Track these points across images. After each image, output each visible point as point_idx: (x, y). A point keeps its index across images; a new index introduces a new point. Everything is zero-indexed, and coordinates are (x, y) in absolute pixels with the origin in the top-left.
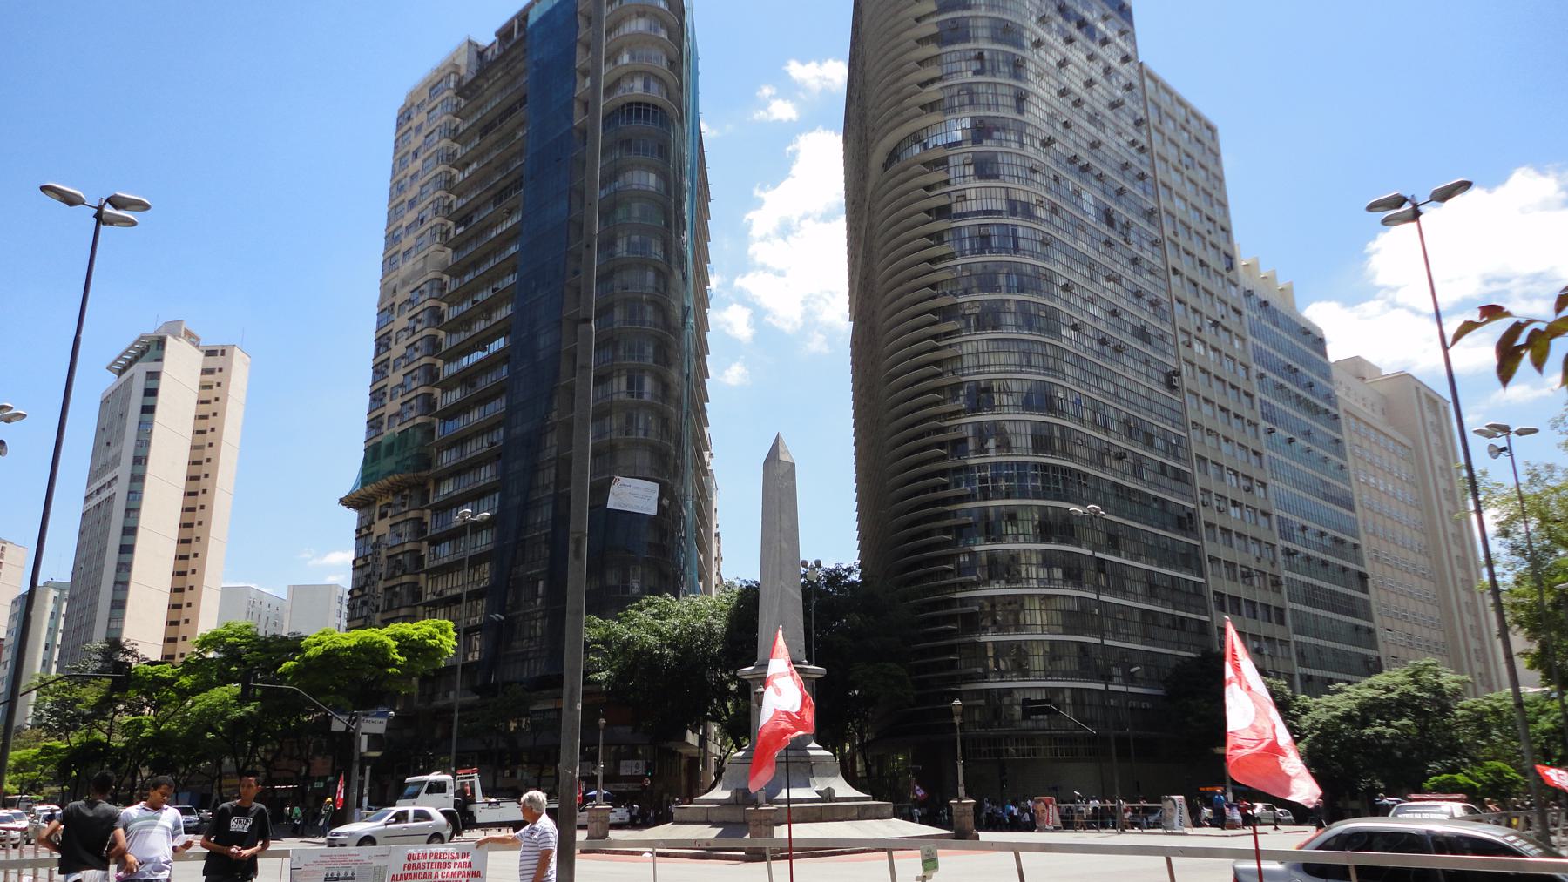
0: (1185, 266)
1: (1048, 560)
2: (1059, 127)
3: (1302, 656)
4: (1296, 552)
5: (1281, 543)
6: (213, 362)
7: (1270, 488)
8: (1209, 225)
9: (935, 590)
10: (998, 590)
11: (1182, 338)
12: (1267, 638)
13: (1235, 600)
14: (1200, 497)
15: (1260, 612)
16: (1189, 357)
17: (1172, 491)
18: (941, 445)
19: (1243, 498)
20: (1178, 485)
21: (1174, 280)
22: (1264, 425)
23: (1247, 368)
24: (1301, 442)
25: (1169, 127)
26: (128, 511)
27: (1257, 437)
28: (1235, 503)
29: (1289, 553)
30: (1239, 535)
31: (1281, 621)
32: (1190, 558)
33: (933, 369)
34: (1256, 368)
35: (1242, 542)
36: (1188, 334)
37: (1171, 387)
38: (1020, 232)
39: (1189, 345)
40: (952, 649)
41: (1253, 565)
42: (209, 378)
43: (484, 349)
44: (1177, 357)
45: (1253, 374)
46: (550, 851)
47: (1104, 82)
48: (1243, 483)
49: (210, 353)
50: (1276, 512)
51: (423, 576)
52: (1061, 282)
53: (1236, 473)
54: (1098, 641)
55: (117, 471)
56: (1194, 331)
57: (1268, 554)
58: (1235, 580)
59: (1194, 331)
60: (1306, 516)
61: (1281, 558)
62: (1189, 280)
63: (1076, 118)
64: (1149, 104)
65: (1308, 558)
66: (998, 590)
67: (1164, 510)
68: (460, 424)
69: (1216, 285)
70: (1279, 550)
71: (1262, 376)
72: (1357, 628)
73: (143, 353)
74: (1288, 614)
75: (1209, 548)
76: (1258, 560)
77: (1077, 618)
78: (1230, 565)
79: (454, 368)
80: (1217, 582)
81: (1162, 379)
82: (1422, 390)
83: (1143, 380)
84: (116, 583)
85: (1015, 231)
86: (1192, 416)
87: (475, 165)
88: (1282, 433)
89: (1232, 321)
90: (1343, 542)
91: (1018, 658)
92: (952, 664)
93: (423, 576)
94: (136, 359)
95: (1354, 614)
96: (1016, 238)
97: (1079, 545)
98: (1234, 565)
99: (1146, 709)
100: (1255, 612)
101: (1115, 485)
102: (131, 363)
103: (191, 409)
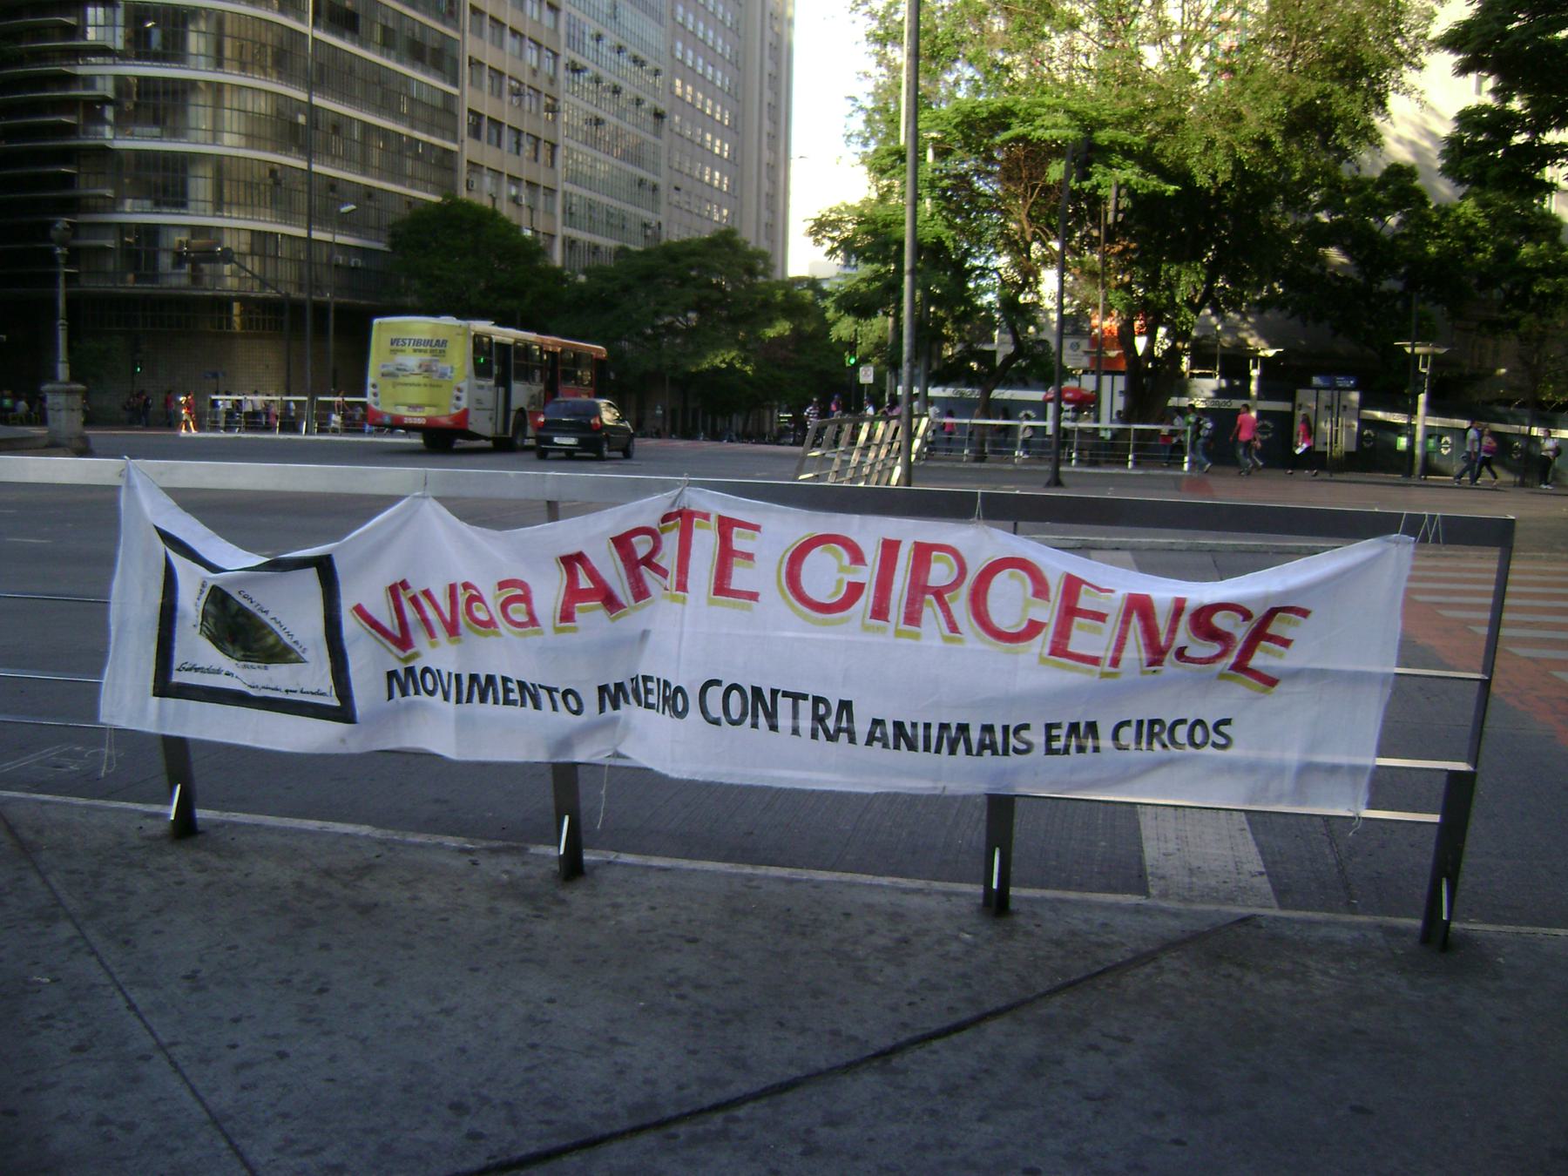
3: (569, 213)
4: (584, 69)
7: (563, 17)
9: (40, 56)
12: (529, 183)
13: (496, 124)
15: (527, 147)
23: (556, 55)
30: (514, 33)
35: (516, 43)
40: (67, 156)
41: (526, 79)
53: (539, 45)
54: (303, 165)
57: (548, 65)
58: (500, 96)
70: (562, 61)
72: (641, 182)
74: (560, 153)
75: (472, 45)
76: (534, 72)
77: (290, 129)
80: (472, 97)
91: (166, 180)
92: (68, 181)
98: (500, 74)
99: (355, 269)
100: (519, 144)
101: (1379, 926)
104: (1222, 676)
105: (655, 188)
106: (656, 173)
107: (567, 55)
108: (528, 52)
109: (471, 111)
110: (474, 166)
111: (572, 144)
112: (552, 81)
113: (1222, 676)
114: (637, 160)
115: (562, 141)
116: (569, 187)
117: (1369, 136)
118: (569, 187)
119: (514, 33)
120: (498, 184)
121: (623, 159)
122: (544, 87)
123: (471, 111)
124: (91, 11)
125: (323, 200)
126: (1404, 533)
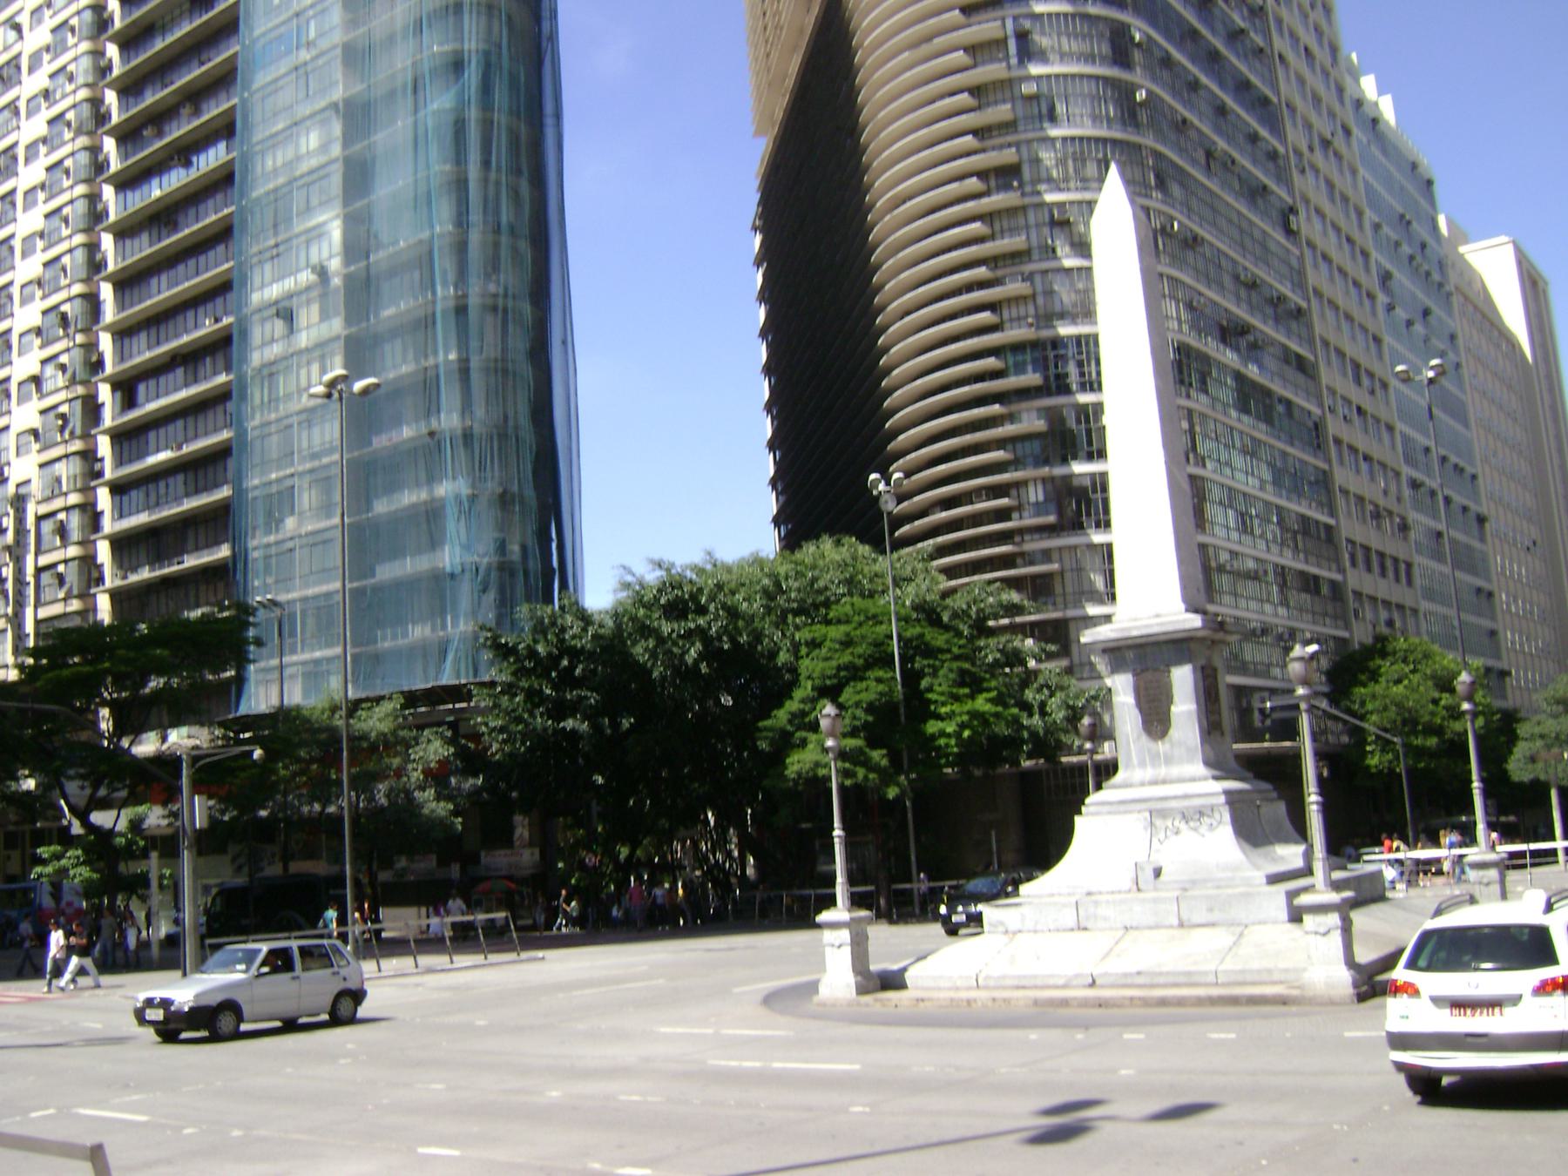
5: (1407, 471)
13: (1367, 549)
14: (1327, 402)
17: (1242, 151)
18: (1000, 444)
22: (1382, 299)
23: (1360, 214)
24: (1418, 328)
27: (1374, 313)
29: (1415, 485)
33: (985, 317)
34: (1370, 216)
37: (1290, 232)
41: (1381, 502)
46: (373, 575)
58: (1364, 521)
61: (1407, 492)
71: (1444, 459)
74: (1416, 572)
76: (1385, 492)
78: (1360, 499)
86: (1312, 278)
88: (1401, 314)
89: (1339, 142)
90: (1462, 470)
93: (85, 46)
95: (1475, 573)
109: (1328, 388)
110: (1358, 595)
112: (1399, 499)
120: (1375, 609)
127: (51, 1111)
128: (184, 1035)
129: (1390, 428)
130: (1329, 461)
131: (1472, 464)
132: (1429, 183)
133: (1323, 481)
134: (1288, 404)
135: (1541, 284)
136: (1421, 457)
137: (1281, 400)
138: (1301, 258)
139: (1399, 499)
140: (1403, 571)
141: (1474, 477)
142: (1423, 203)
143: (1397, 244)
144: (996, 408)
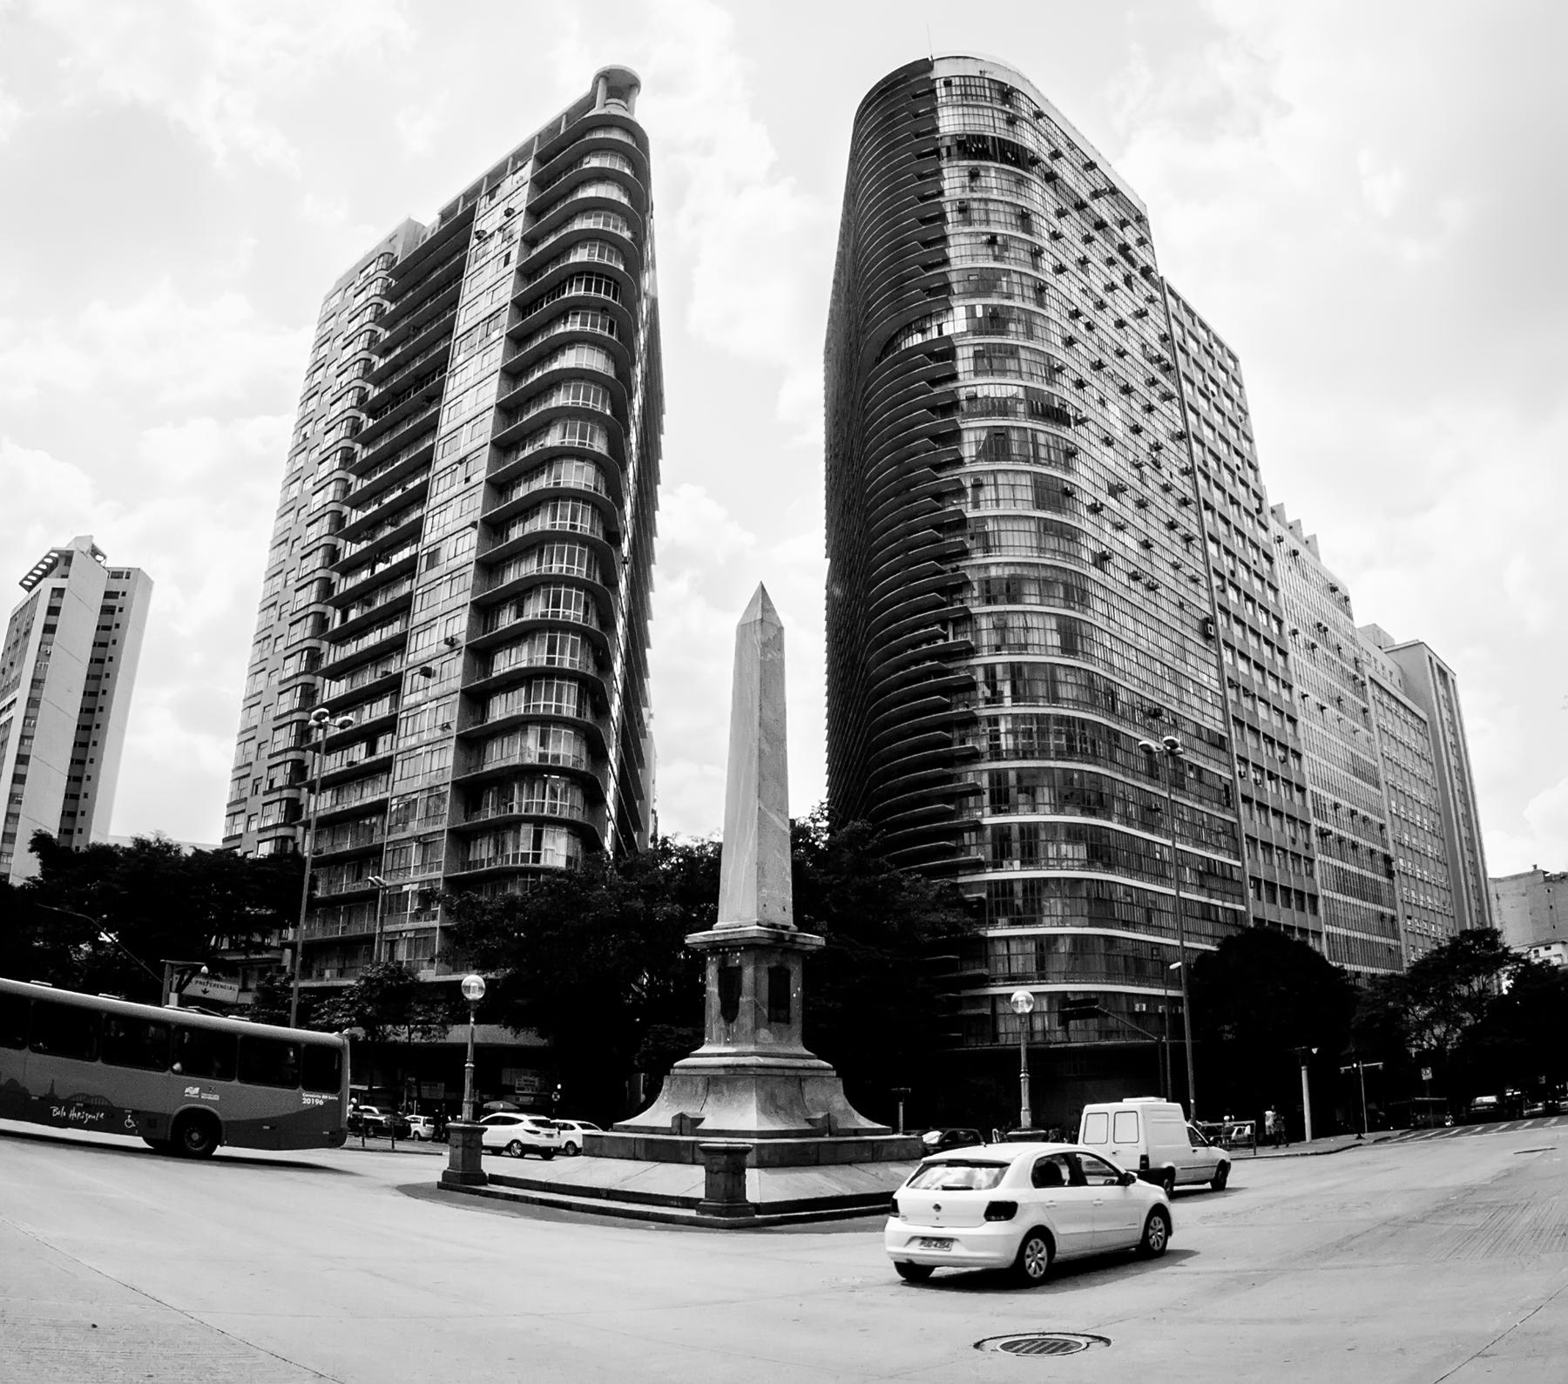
0: (1217, 498)
1: (1075, 834)
2: (1082, 327)
4: (1330, 833)
6: (117, 586)
7: (1308, 793)
8: (1238, 460)
10: (1014, 872)
11: (1216, 581)
14: (1237, 768)
16: (1224, 604)
19: (1279, 771)
20: (1213, 752)
21: (1207, 515)
23: (1308, 825)
24: (1332, 711)
25: (1192, 345)
26: (23, 737)
28: (1271, 776)
29: (1323, 834)
31: (1315, 911)
32: (1232, 837)
36: (1222, 577)
37: (1207, 637)
38: (1041, 438)
39: (1224, 591)
42: (111, 602)
43: (387, 561)
44: (1212, 601)
45: (1287, 629)
47: (1125, 288)
48: (1279, 753)
49: (116, 575)
50: (1309, 787)
51: (301, 829)
52: (1089, 501)
55: (16, 694)
56: (1227, 575)
57: (1301, 836)
59: (1227, 575)
60: (1337, 791)
61: (1314, 839)
62: (1221, 516)
63: (1097, 320)
64: (1173, 321)
65: (1341, 840)
66: (1014, 872)
67: (1200, 780)
68: (352, 649)
69: (1247, 525)
70: (1313, 829)
72: (1382, 916)
73: (51, 567)
74: (1321, 902)
76: (1294, 841)
79: (351, 583)
81: (1196, 625)
82: (1435, 660)
83: (1177, 625)
84: (8, 814)
85: (1034, 437)
87: (398, 351)
94: (46, 574)
96: (1036, 445)
97: (1110, 819)
102: (40, 578)
103: (89, 634)
104: (413, 1190)
105: (1393, 919)
106: (1394, 908)
107: (1315, 822)
108: (1286, 826)
109: (1251, 878)
111: (1328, 893)
112: (1307, 846)
113: (413, 1190)
114: (1377, 900)
115: (1322, 892)
116: (1330, 929)
117: (699, 876)
118: (1330, 929)
119: (1251, 728)
121: (369, 939)
122: (1303, 852)
123: (1251, 878)
124: (561, 863)
125: (1141, 963)
126: (1316, 1135)
127: (216, 1097)
128: (220, 1151)
129: (1301, 789)
130: (1238, 816)
131: (1385, 846)
132: (1347, 599)
133: (1231, 831)
134: (1200, 770)
135: (1450, 676)
136: (1330, 811)
137: (1192, 766)
138: (1220, 657)
139: (1307, 846)
140: (1307, 900)
141: (1382, 827)
142: (1342, 615)
143: (1314, 646)
144: (692, 1213)
